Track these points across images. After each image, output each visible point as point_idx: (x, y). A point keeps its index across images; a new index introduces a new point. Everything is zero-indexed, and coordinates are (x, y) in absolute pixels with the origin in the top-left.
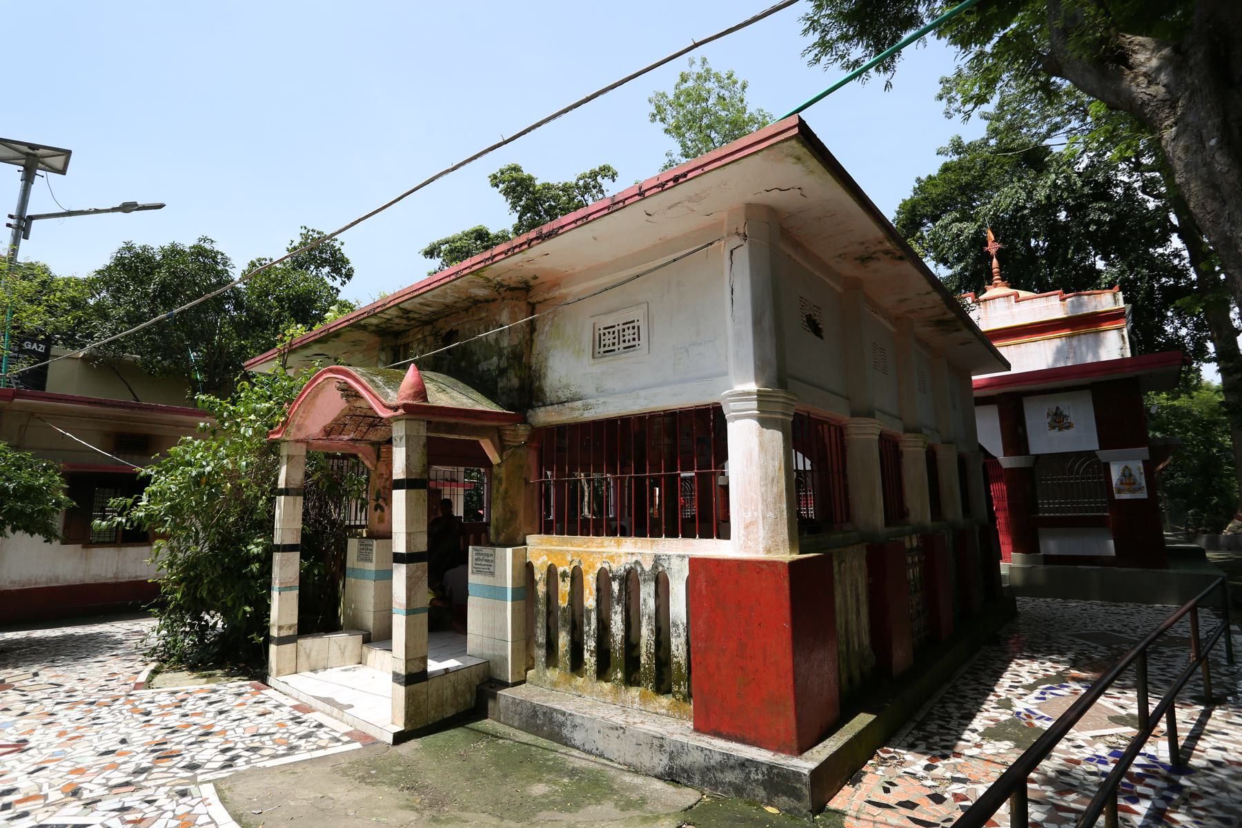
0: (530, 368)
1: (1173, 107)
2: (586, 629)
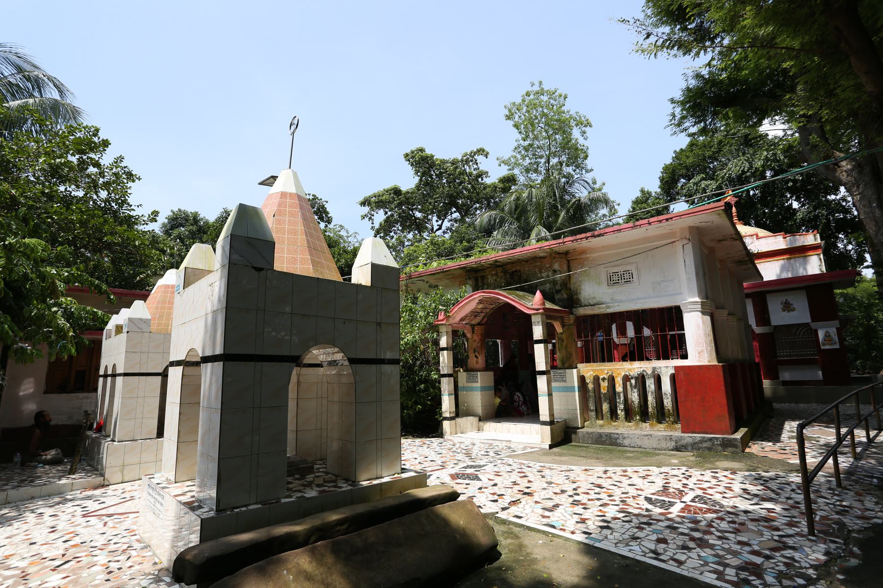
0: (570, 289)
1: (858, 187)
2: (618, 400)
